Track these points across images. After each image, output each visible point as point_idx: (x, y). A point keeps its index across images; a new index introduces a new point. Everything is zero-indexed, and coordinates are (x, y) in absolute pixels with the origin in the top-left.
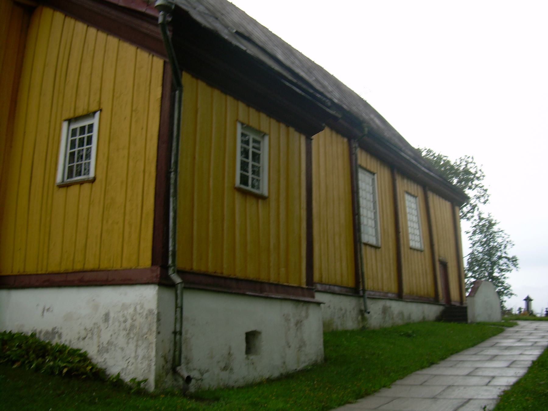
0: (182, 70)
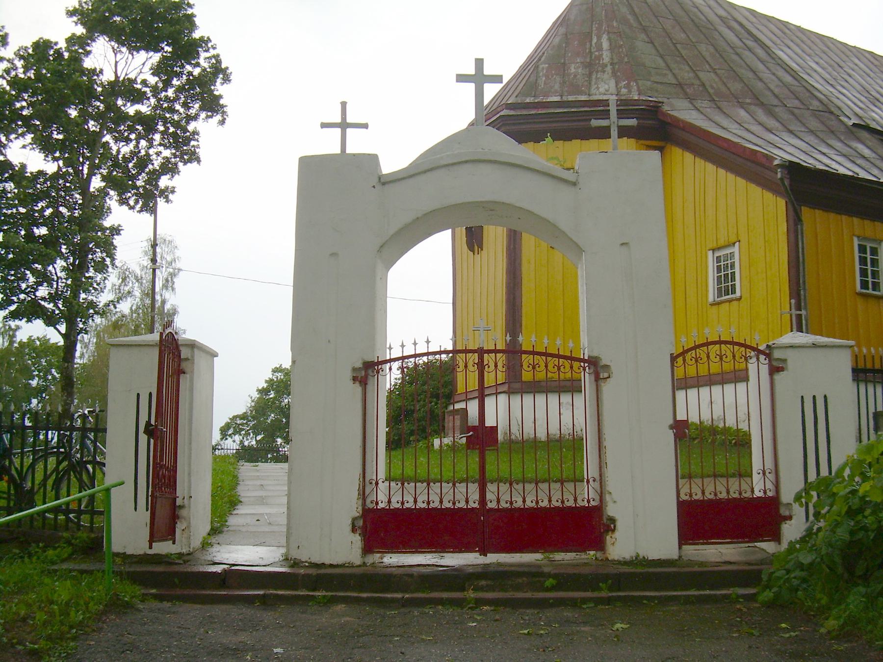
0: (801, 206)
